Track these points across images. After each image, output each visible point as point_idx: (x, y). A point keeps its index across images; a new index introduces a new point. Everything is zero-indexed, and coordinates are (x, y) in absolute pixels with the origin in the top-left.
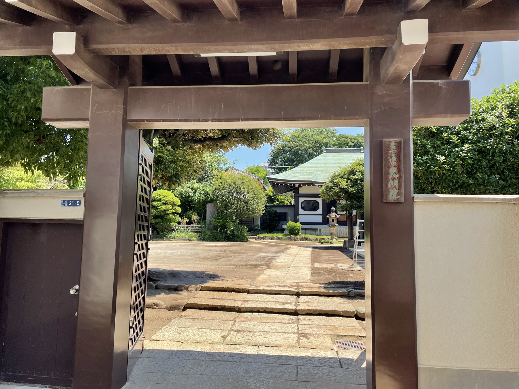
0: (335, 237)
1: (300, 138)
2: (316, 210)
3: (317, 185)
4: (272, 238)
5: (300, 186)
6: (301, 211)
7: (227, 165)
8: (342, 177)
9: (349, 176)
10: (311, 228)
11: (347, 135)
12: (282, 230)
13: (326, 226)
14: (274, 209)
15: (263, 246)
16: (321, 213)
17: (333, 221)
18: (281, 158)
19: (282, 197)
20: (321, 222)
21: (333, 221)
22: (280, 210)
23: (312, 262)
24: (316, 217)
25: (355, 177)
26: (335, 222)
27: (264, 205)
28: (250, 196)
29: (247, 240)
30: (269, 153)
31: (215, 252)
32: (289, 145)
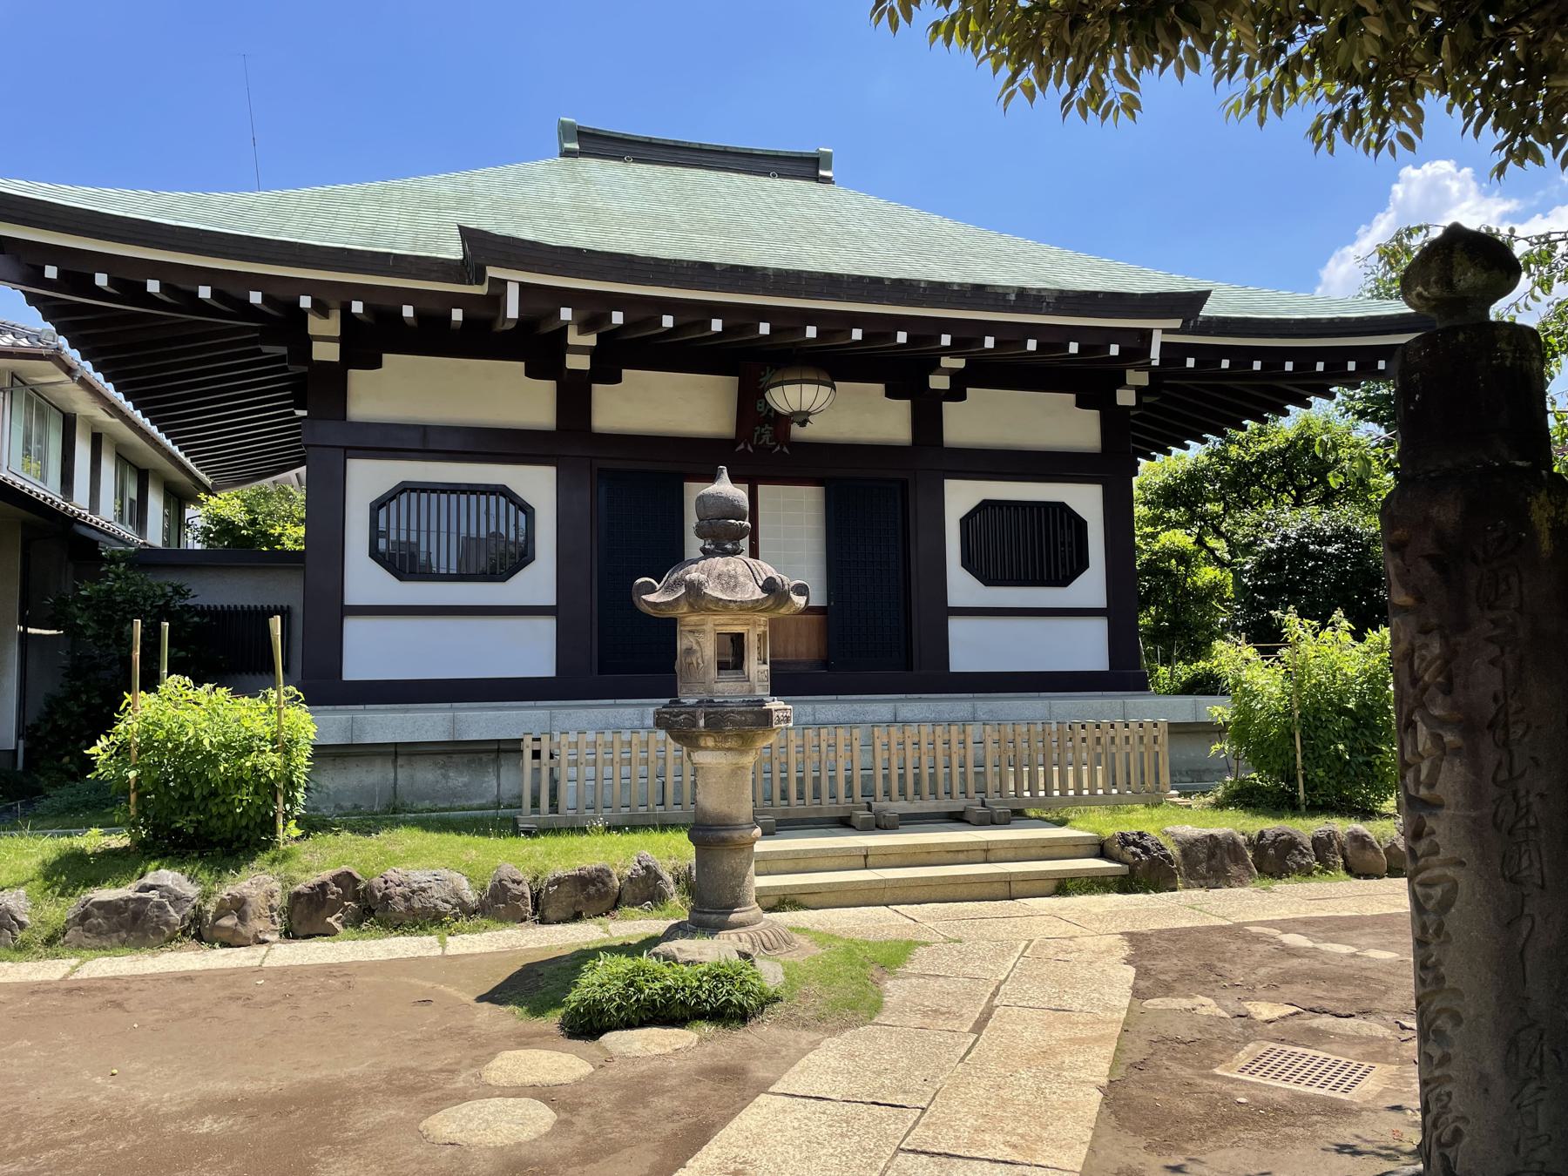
2: (1064, 581)
6: (364, 579)
16: (549, 598)
17: (733, 655)
21: (733, 655)
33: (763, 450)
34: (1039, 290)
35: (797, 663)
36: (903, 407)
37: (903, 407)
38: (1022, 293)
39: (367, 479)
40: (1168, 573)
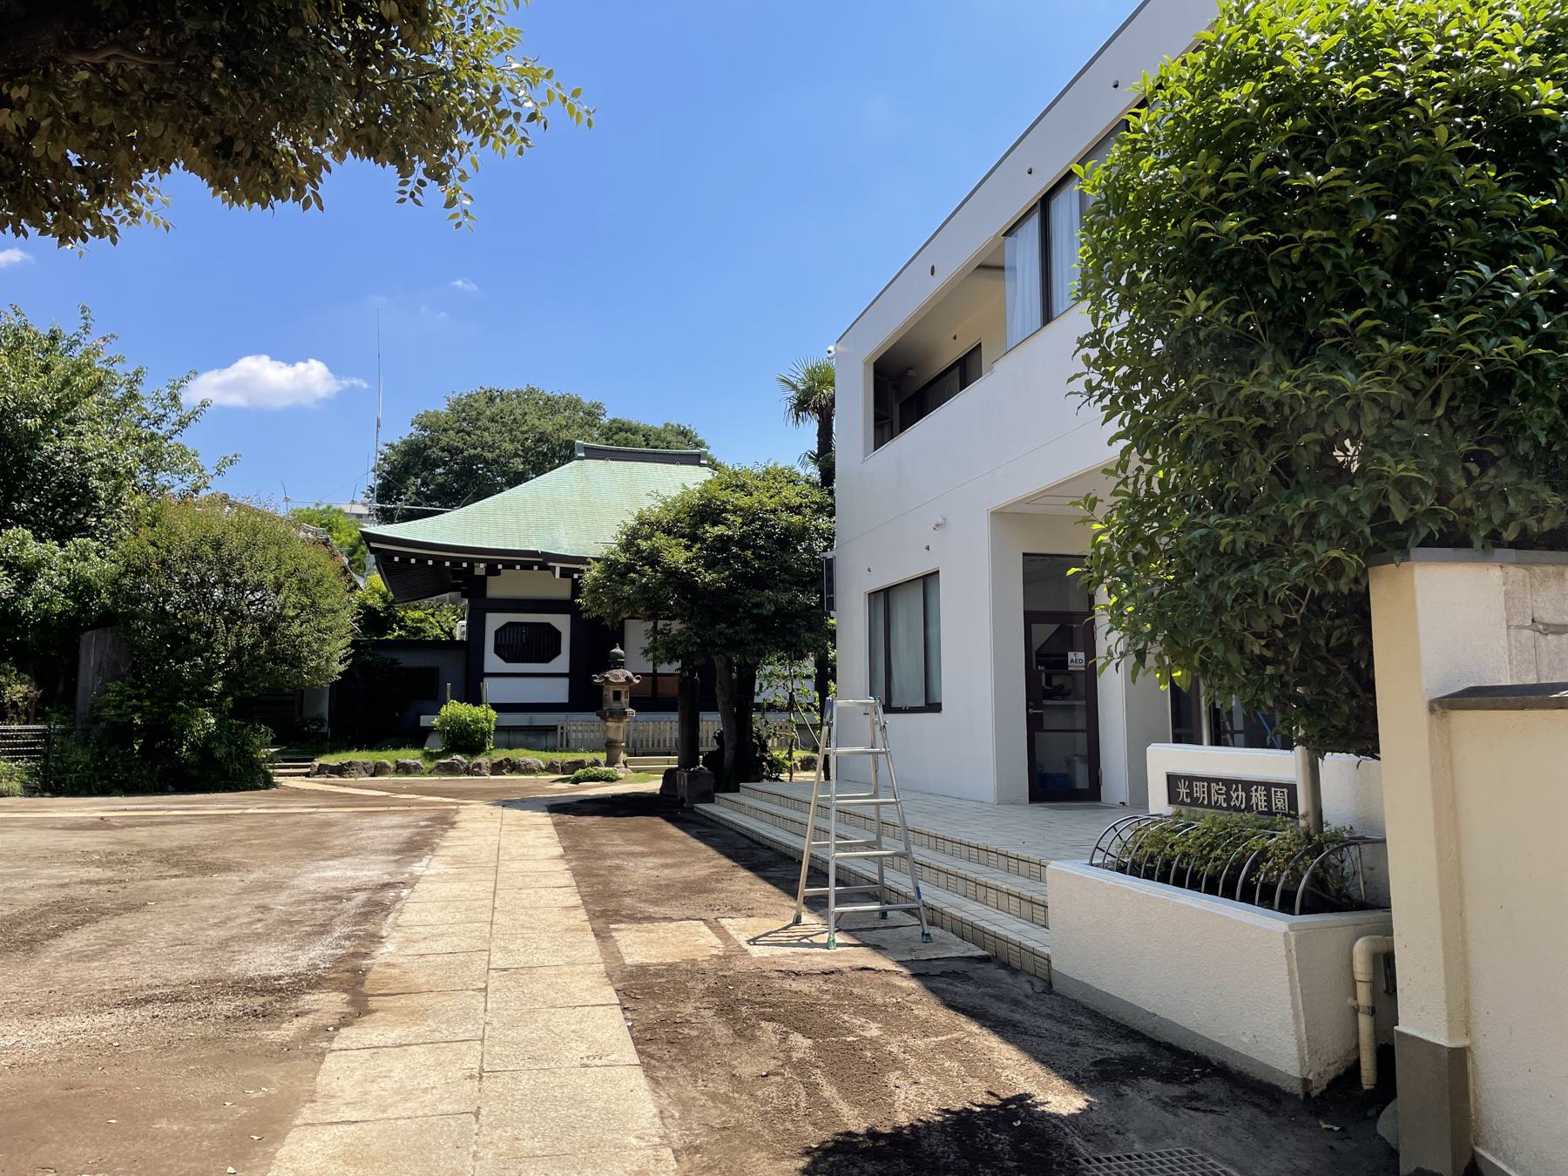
0: (623, 756)
1: (483, 422)
2: (547, 659)
3: (558, 566)
4: (379, 770)
5: (492, 570)
6: (492, 662)
7: (190, 479)
8: (668, 532)
9: (694, 526)
10: (529, 728)
11: (634, 423)
12: (417, 738)
13: (593, 716)
14: (388, 655)
15: (335, 814)
17: (617, 695)
18: (414, 483)
19: (417, 614)
20: (565, 700)
22: (408, 660)
23: (593, 916)
24: (548, 684)
25: (720, 530)
26: (625, 700)
27: (349, 639)
28: (288, 599)
29: (268, 783)
30: (373, 465)
31: (69, 873)
32: (444, 440)
39: (495, 621)
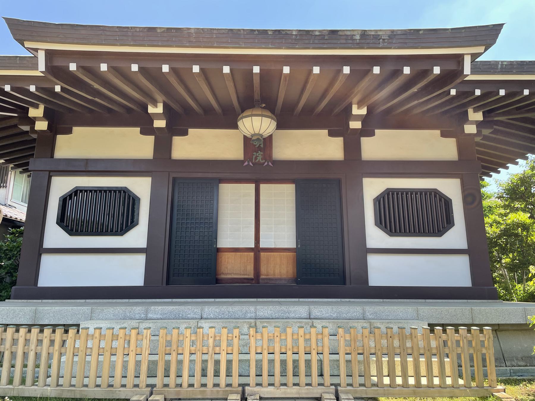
6: (54, 235)
16: (142, 243)
33: (258, 166)
34: (376, 31)
35: (280, 279)
36: (339, 142)
37: (339, 142)
38: (364, 34)
40: (517, 235)
